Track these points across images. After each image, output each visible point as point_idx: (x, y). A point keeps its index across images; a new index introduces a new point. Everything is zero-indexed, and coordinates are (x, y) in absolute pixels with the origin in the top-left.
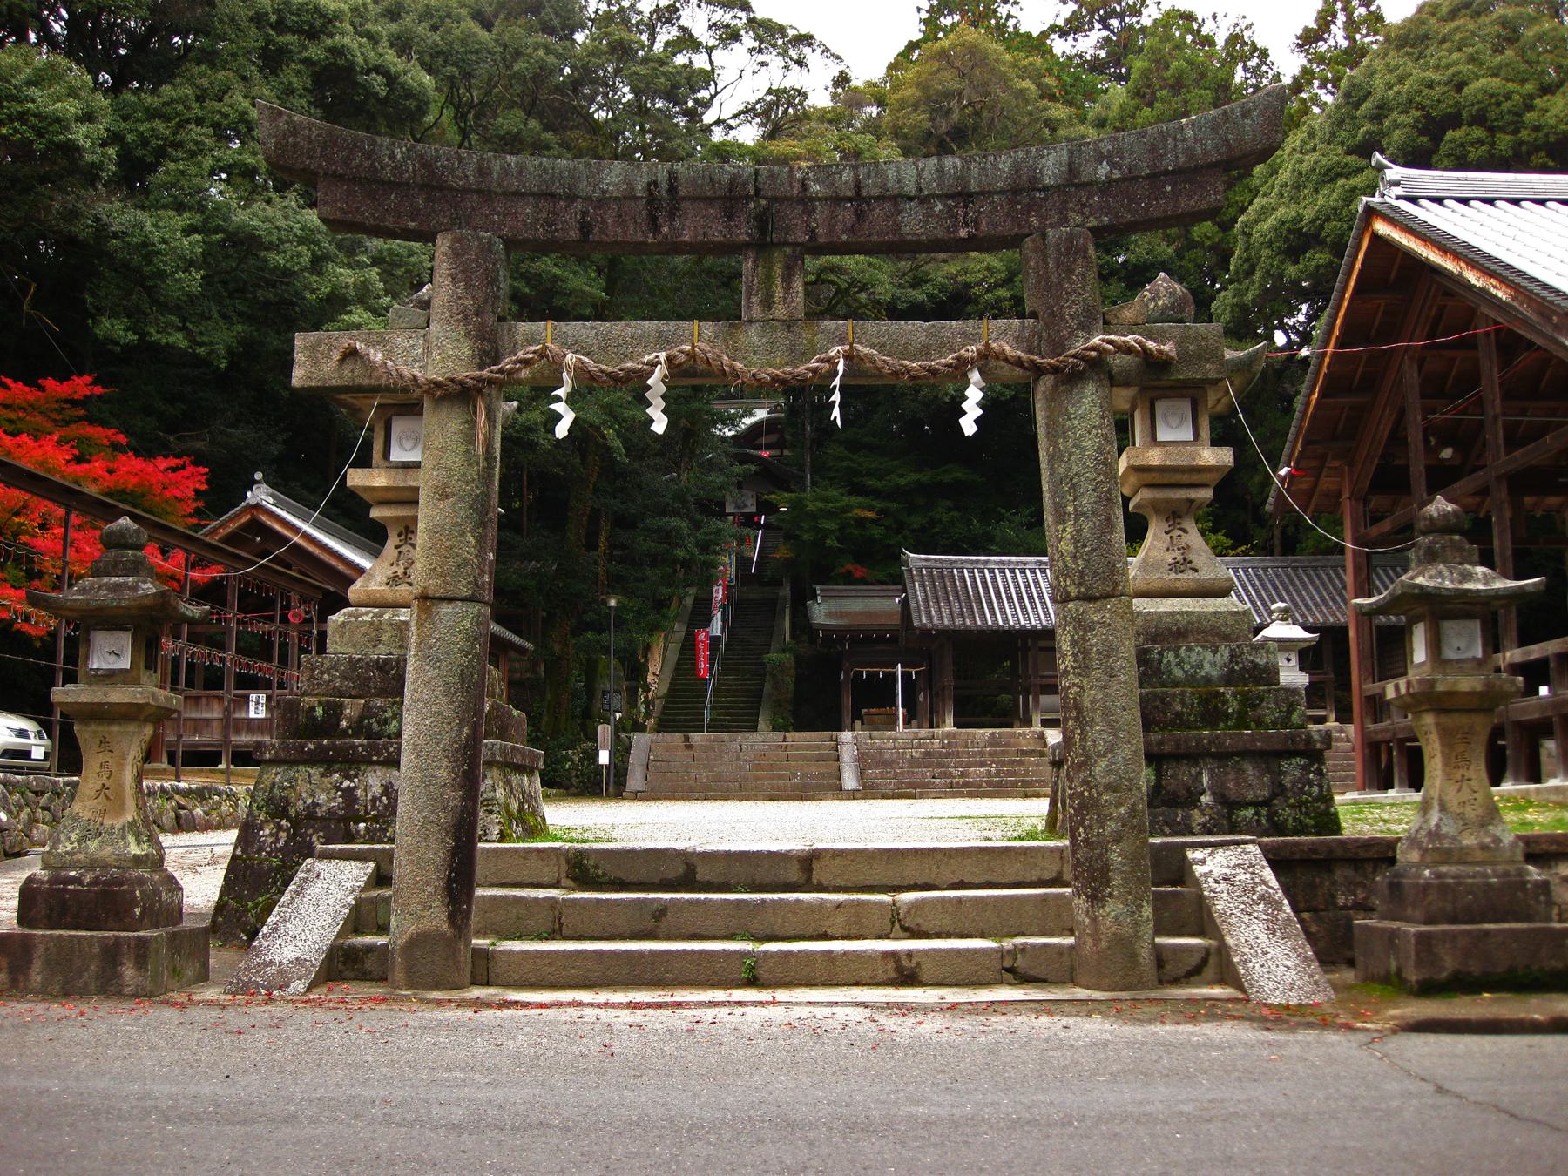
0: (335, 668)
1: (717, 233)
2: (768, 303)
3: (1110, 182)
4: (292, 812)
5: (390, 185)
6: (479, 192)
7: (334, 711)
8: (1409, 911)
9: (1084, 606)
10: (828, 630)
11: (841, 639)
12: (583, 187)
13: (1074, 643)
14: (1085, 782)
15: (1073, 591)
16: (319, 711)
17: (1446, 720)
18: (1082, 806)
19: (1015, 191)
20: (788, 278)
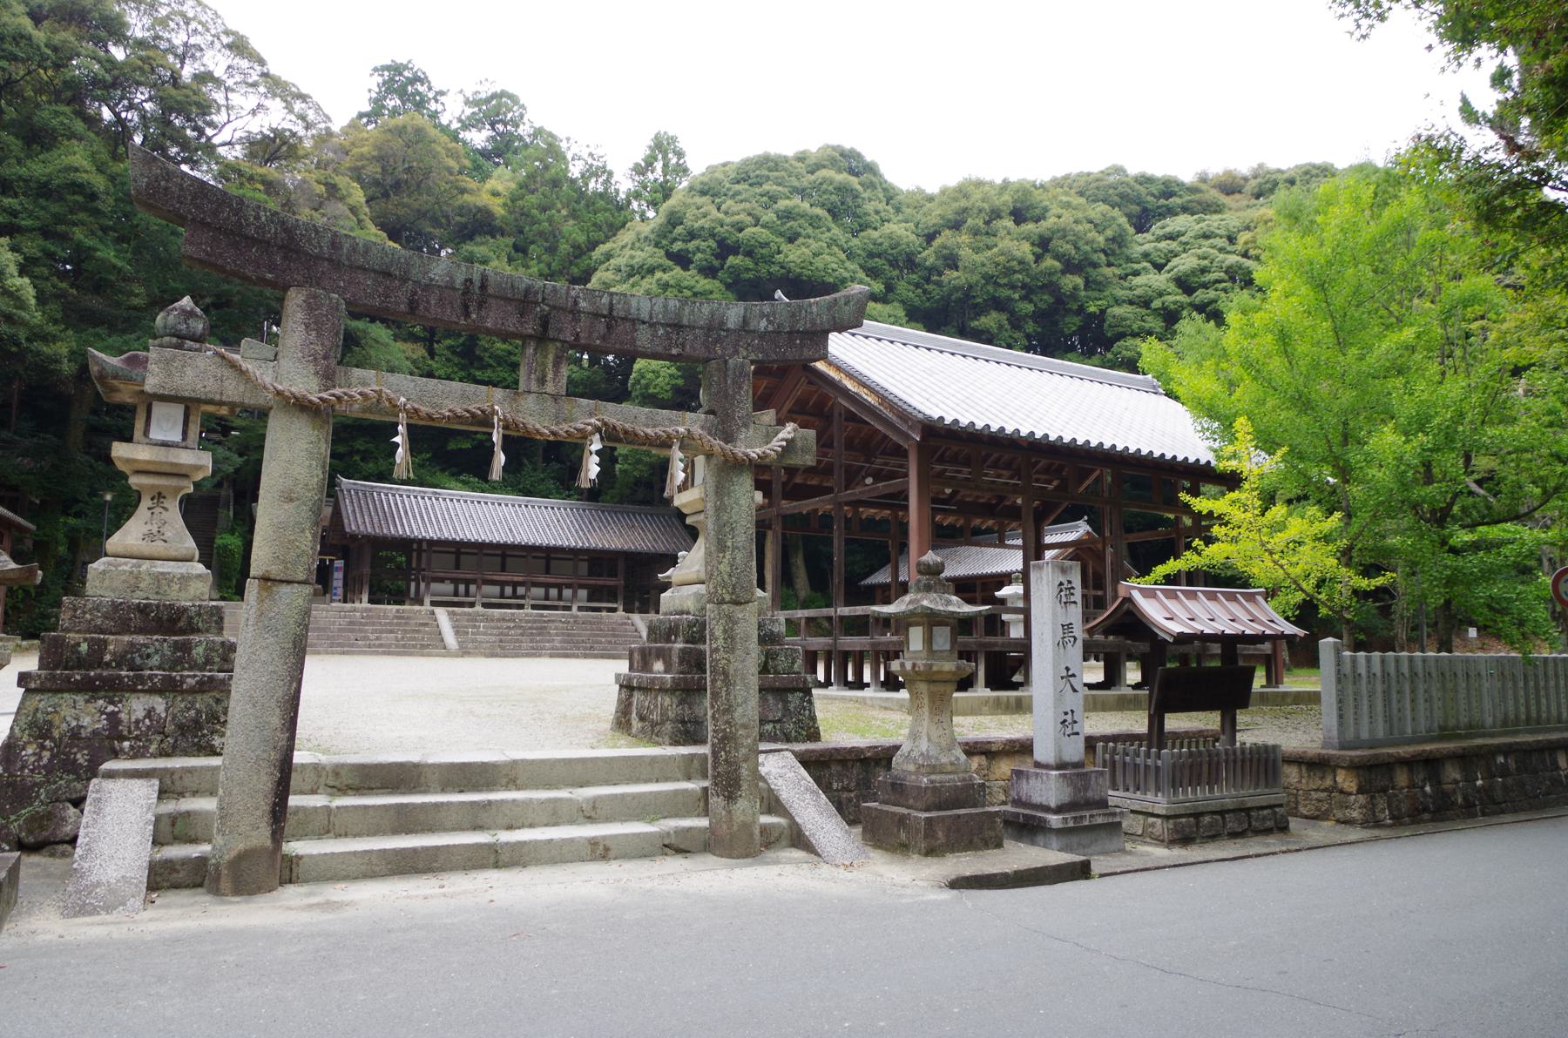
0: (97, 608)
1: (511, 324)
2: (542, 381)
3: (766, 332)
4: (56, 734)
5: (253, 241)
6: (330, 260)
7: (99, 647)
8: (911, 802)
9: (732, 608)
12: (415, 273)
13: (725, 631)
14: (727, 722)
15: (727, 597)
16: (84, 647)
17: (934, 688)
18: (724, 738)
19: (709, 329)
20: (557, 365)
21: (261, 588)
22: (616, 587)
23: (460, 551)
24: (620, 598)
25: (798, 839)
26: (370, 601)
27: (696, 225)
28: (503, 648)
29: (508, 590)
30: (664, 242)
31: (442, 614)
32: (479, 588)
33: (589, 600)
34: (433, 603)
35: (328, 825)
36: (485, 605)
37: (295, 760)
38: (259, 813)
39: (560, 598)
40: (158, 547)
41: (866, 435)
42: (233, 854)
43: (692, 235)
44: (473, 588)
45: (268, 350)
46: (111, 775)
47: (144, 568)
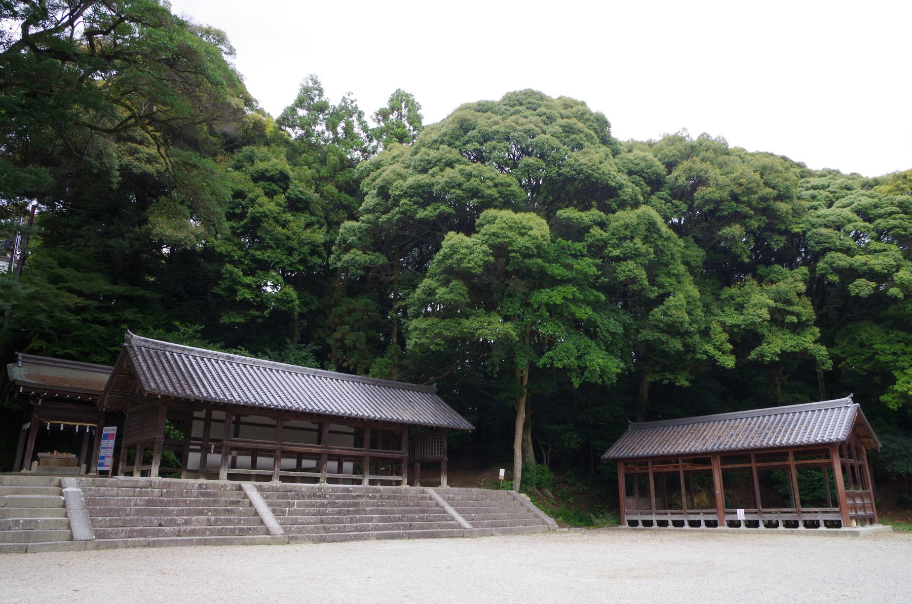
10: (27, 387)
11: (37, 396)
26: (162, 474)
27: (490, 130)
28: (327, 530)
30: (457, 143)
31: (249, 487)
36: (283, 479)
39: (254, 465)
43: (486, 138)
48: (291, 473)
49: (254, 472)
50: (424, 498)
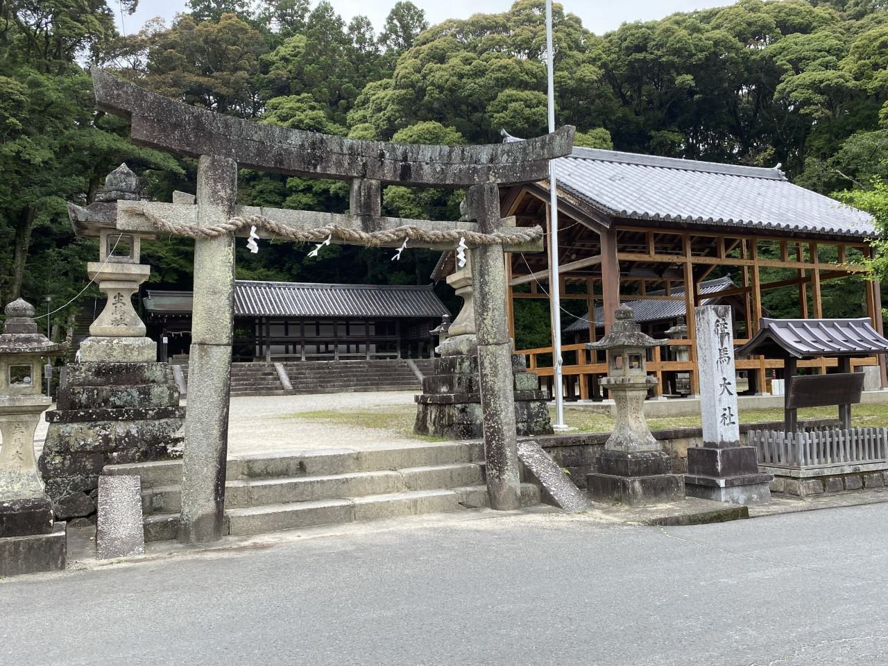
10: (156, 313)
11: (163, 317)
13: (491, 363)
21: (202, 350)
22: (395, 342)
23: (287, 321)
24: (398, 348)
25: (546, 499)
29: (322, 347)
32: (303, 347)
33: (377, 352)
34: (273, 359)
35: (250, 499)
37: (228, 459)
38: (208, 491)
39: (358, 351)
40: (122, 329)
41: (585, 229)
42: (195, 518)
44: (298, 347)
45: (190, 197)
46: (111, 473)
47: (115, 342)
48: (314, 355)
49: (349, 355)
50: (404, 366)
